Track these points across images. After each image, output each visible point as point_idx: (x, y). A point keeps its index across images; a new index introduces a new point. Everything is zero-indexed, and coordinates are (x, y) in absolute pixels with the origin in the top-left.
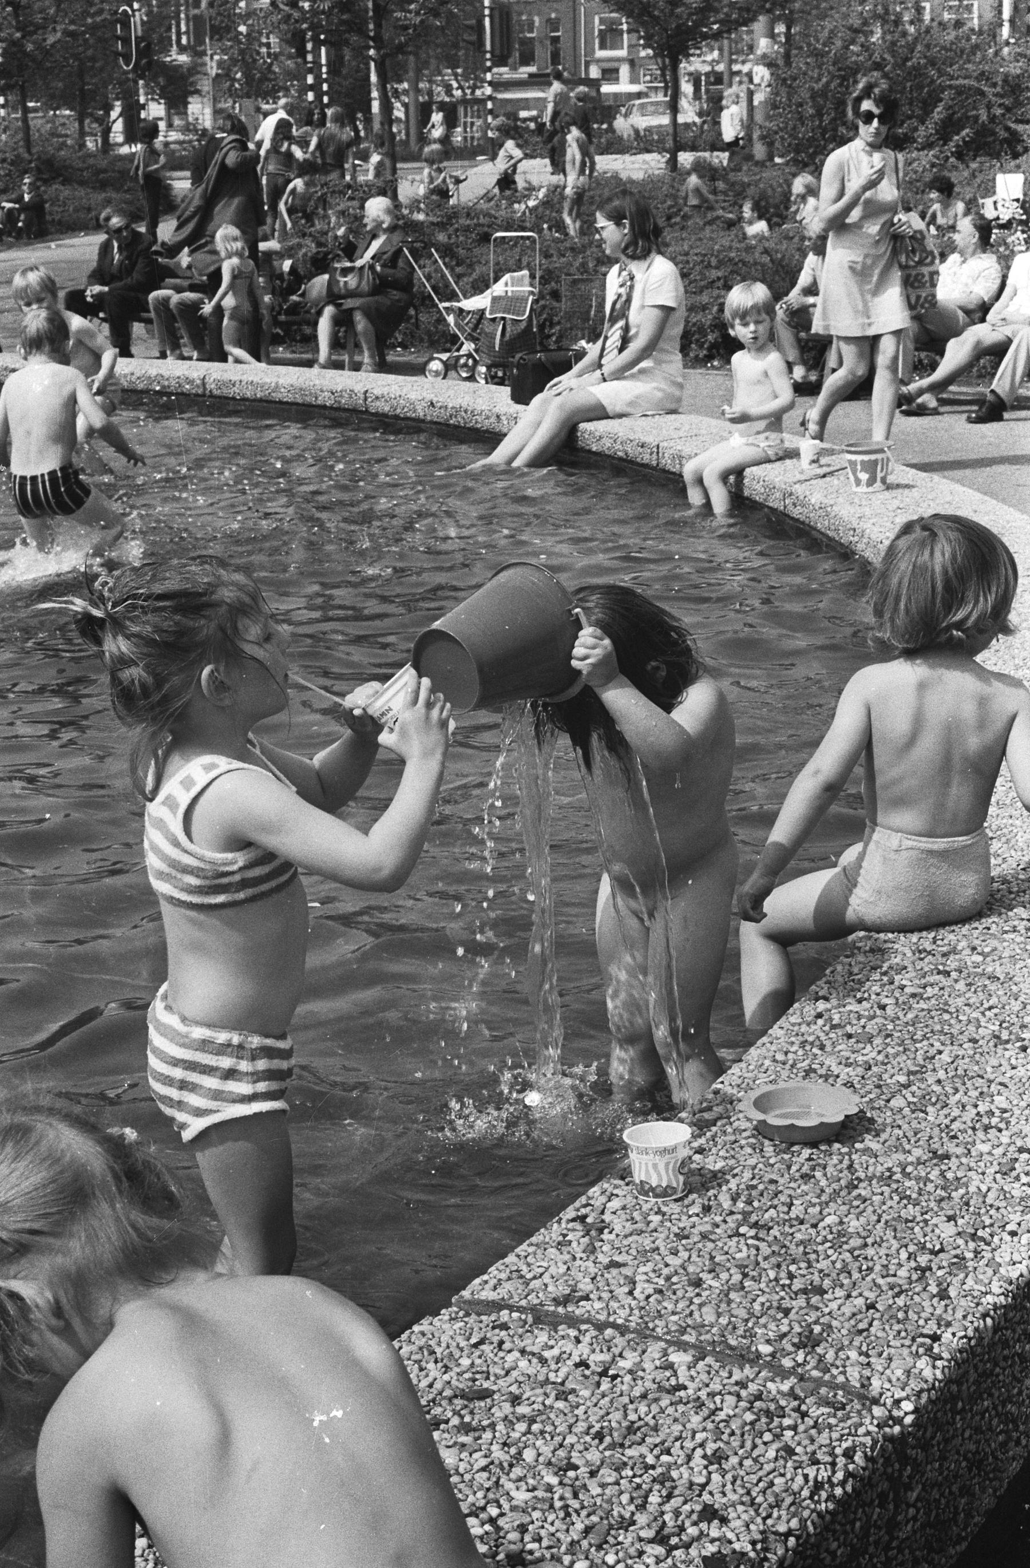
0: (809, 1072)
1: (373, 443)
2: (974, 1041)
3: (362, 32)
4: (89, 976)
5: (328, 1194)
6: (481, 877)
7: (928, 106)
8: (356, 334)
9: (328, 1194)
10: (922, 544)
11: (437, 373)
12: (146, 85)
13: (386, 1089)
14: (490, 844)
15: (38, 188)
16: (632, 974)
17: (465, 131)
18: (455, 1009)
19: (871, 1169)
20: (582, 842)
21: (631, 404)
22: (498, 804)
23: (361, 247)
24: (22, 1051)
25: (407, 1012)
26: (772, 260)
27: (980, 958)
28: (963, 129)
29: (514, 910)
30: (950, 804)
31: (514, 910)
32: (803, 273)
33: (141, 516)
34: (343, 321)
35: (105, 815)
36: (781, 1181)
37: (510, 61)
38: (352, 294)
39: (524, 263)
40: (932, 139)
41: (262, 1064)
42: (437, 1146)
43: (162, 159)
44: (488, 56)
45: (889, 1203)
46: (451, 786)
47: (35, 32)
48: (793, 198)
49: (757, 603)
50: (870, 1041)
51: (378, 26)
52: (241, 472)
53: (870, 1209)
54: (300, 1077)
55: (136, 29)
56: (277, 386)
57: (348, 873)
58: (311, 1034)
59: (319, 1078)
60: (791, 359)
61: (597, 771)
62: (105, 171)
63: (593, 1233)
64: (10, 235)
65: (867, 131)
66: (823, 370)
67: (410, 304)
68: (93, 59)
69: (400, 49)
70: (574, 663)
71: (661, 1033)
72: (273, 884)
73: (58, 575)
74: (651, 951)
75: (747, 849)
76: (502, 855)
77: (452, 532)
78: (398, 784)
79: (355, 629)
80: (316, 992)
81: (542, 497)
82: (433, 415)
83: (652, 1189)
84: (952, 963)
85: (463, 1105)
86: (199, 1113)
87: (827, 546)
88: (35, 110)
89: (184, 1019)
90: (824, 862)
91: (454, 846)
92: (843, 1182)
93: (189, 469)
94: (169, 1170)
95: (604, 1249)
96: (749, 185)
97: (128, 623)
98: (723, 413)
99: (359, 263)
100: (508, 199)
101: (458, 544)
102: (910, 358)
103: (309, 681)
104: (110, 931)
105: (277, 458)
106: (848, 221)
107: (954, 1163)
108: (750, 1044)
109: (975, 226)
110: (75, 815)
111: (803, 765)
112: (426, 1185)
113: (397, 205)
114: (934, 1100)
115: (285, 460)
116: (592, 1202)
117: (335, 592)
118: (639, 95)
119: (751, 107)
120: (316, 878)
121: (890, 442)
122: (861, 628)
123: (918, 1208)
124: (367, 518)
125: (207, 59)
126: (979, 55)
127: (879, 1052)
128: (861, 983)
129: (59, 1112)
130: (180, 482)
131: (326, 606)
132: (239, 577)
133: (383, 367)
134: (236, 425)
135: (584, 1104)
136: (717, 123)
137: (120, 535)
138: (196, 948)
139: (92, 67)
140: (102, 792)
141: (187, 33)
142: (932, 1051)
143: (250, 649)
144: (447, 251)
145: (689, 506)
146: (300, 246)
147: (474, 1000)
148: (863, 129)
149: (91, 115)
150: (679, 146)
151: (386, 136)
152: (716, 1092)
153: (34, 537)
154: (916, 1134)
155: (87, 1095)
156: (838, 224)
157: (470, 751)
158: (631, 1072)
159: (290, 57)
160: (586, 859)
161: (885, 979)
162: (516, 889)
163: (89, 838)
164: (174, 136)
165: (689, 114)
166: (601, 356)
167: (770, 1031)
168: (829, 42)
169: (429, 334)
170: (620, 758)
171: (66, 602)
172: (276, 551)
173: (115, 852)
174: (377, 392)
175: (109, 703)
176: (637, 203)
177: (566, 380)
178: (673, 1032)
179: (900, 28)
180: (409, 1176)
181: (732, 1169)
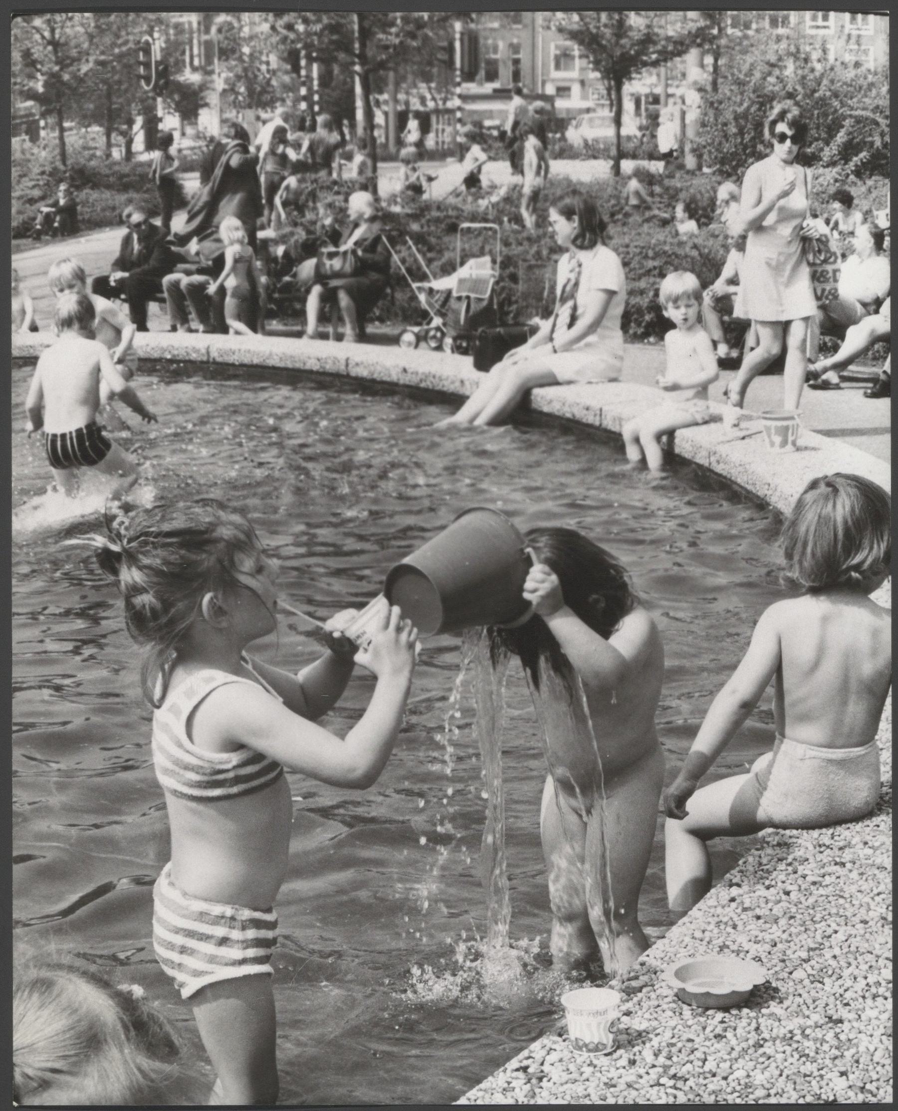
0: (722, 948)
1: (354, 403)
2: (865, 922)
3: (349, 50)
4: (104, 856)
5: (306, 1045)
6: (441, 777)
7: (832, 129)
8: (339, 309)
9: (306, 1045)
10: (826, 498)
11: (409, 344)
12: (164, 101)
13: (357, 957)
14: (450, 749)
15: (71, 193)
16: (571, 862)
17: (437, 136)
18: (417, 890)
19: (775, 1031)
20: (530, 749)
21: (578, 372)
22: (458, 715)
23: (346, 233)
24: (48, 916)
25: (377, 892)
26: (701, 255)
27: (870, 851)
28: (861, 151)
29: (470, 806)
30: (848, 720)
31: (470, 806)
32: (726, 266)
33: (153, 466)
34: (329, 298)
35: (118, 719)
36: (697, 1040)
37: (478, 78)
38: (337, 275)
39: (487, 248)
40: (835, 158)
41: (251, 934)
42: (400, 1005)
43: (176, 164)
44: (458, 73)
45: (790, 1060)
46: (417, 699)
47: (71, 65)
48: (718, 203)
49: (684, 546)
50: (776, 921)
51: (363, 45)
52: (238, 427)
53: (773, 1065)
54: (283, 945)
55: (157, 54)
56: (271, 354)
57: (326, 772)
58: (293, 908)
59: (299, 946)
60: (716, 338)
61: (544, 687)
62: (128, 175)
63: (534, 1081)
64: (47, 234)
65: (782, 150)
66: (743, 348)
67: (388, 283)
68: (120, 82)
69: (382, 65)
70: (526, 595)
71: (596, 913)
72: (262, 780)
73: (83, 516)
74: (587, 842)
75: (673, 756)
76: (460, 759)
77: (421, 480)
78: (370, 697)
79: (335, 563)
80: (298, 873)
81: (500, 451)
82: (404, 379)
83: (586, 1045)
84: (847, 856)
85: (423, 971)
86: (197, 974)
87: (746, 498)
88: (71, 129)
89: (185, 894)
90: (738, 768)
91: (419, 750)
92: (751, 1042)
93: (195, 425)
94: (170, 1022)
95: (543, 1094)
96: (681, 190)
97: (140, 556)
98: (657, 382)
99: (343, 248)
100: (473, 195)
101: (428, 491)
102: (816, 343)
103: (295, 607)
104: (122, 818)
105: (271, 415)
106: (765, 223)
107: (846, 1026)
108: (672, 924)
109: (871, 233)
110: (96, 719)
111: (722, 685)
112: (390, 1039)
113: (377, 200)
114: (830, 972)
115: (278, 418)
116: (533, 1055)
117: (318, 531)
118: (588, 110)
119: (683, 126)
120: (298, 776)
121: (800, 411)
122: (774, 568)
123: (815, 1064)
124: (347, 468)
125: (215, 77)
126: (874, 92)
127: (784, 931)
128: (769, 872)
129: (78, 970)
130: (187, 437)
131: (310, 544)
132: (236, 518)
133: (362, 337)
134: (235, 387)
135: (528, 972)
136: (654, 136)
137: (135, 482)
138: (196, 833)
139: (119, 89)
140: (117, 700)
141: (199, 55)
142: (829, 931)
143: (244, 579)
144: (419, 239)
145: (626, 461)
146: (292, 234)
147: (434, 882)
148: (777, 146)
149: (117, 129)
150: (621, 155)
151: (368, 139)
152: (643, 964)
153: (64, 485)
154: (814, 1001)
155: (101, 957)
156: (757, 226)
157: (433, 670)
158: (569, 946)
159: (287, 72)
160: (533, 763)
161: (790, 869)
162: (472, 788)
163: (104, 739)
164: (187, 143)
165: (631, 126)
166: (553, 331)
167: (690, 913)
168: (750, 73)
169: (403, 310)
170: (564, 677)
171: (89, 539)
172: (266, 496)
173: (127, 752)
174: (357, 359)
175: (123, 626)
176: (585, 202)
177: (521, 352)
178: (607, 913)
179: (809, 65)
180: (376, 1031)
181: (655, 1029)
